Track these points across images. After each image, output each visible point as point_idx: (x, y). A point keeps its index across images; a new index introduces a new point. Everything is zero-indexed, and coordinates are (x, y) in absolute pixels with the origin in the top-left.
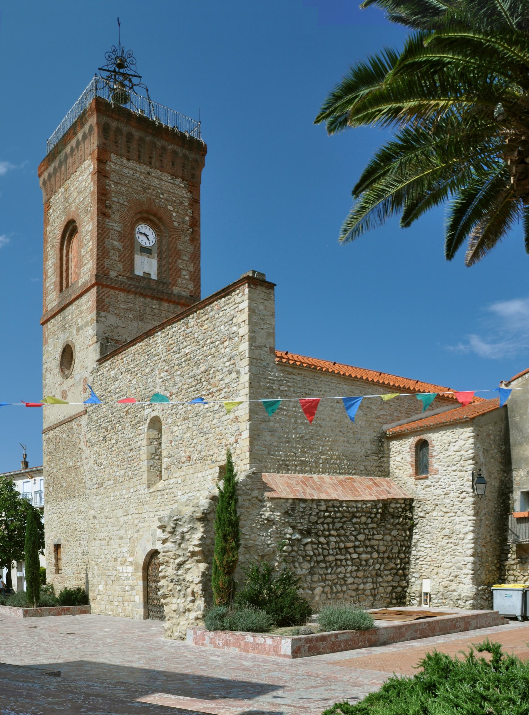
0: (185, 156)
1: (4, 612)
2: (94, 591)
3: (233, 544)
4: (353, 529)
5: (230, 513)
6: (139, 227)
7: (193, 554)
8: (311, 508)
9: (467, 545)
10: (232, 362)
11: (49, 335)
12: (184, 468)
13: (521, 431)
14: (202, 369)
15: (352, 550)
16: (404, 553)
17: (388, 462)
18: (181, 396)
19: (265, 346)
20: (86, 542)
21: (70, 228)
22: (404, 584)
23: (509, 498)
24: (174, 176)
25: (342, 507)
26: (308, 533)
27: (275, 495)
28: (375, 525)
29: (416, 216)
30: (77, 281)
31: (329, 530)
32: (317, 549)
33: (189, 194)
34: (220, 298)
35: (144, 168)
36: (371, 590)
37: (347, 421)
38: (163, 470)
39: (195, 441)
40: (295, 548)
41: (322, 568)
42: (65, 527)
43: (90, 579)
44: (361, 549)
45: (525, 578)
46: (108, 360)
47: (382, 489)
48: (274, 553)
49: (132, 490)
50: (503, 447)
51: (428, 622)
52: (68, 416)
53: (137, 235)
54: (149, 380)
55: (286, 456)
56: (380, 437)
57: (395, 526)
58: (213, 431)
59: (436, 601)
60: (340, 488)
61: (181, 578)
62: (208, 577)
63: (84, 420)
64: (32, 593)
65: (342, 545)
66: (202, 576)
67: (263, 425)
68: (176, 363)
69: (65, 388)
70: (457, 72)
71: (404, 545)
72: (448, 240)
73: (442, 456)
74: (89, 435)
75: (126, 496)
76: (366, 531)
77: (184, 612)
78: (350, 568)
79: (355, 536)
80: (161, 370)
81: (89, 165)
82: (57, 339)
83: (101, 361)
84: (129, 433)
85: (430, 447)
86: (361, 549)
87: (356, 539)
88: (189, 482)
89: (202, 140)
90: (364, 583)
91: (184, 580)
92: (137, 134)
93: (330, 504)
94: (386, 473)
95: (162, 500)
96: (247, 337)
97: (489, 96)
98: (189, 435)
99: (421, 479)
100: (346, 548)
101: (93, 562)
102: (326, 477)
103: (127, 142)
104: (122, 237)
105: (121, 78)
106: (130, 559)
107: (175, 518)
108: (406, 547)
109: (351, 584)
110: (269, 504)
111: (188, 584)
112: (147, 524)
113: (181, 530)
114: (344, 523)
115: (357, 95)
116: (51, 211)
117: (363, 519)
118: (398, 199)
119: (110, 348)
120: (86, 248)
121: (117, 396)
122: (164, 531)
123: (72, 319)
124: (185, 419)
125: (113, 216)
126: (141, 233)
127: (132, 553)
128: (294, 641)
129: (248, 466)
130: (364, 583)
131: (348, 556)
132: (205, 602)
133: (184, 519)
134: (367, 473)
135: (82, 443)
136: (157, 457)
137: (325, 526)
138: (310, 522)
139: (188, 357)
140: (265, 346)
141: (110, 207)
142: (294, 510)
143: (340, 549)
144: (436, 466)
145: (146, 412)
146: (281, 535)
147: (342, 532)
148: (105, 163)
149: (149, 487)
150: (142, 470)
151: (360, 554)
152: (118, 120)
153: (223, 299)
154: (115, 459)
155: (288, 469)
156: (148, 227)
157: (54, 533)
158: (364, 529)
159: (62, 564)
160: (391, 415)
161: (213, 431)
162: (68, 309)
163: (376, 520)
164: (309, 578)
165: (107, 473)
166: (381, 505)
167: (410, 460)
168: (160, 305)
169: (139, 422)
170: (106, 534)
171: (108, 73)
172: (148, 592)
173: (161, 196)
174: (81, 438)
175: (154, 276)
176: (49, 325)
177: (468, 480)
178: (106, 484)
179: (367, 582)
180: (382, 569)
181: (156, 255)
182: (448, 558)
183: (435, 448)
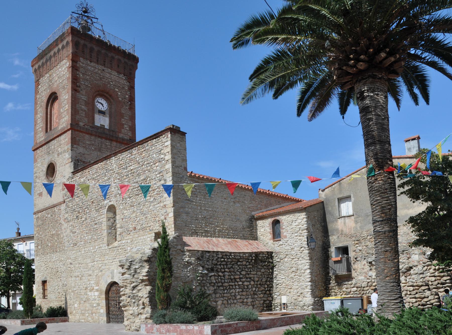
0: (125, 62)
1: (6, 323)
2: (71, 308)
3: (169, 274)
5: (166, 257)
6: (98, 99)
7: (143, 281)
8: (213, 256)
9: (307, 275)
10: (161, 174)
11: (38, 157)
12: (132, 234)
13: (333, 215)
14: (142, 178)
15: (238, 280)
16: (269, 282)
17: (256, 232)
18: (128, 193)
19: (181, 166)
20: (65, 279)
21: (53, 97)
22: (271, 299)
23: (328, 251)
24: (119, 73)
25: (231, 256)
26: (212, 270)
27: (191, 249)
29: (281, 94)
30: (58, 127)
31: (224, 269)
32: (218, 279)
34: (153, 139)
35: (101, 67)
36: (251, 302)
37: (231, 209)
38: (117, 236)
39: (138, 219)
40: (205, 278)
41: (221, 290)
42: (50, 270)
43: (68, 301)
44: (244, 280)
45: (341, 293)
46: (79, 172)
48: (192, 281)
49: (97, 247)
50: (323, 224)
51: (289, 317)
52: (52, 204)
53: (96, 104)
55: (196, 227)
57: (263, 266)
58: (150, 213)
59: (290, 307)
60: (229, 246)
61: (135, 295)
62: (152, 294)
63: (63, 207)
64: (28, 310)
65: (232, 277)
66: (149, 294)
67: (182, 210)
70: (306, 24)
71: (269, 277)
72: (298, 107)
73: (288, 228)
74: (66, 215)
75: (93, 251)
76: (246, 270)
77: (138, 315)
78: (238, 290)
79: (240, 272)
80: (115, 178)
81: (66, 63)
83: (74, 173)
84: (94, 214)
85: (281, 224)
86: (244, 280)
88: (135, 242)
89: (135, 54)
90: (247, 299)
91: (137, 296)
92: (96, 48)
93: (224, 254)
94: (255, 238)
95: (118, 252)
96: (170, 161)
97: (323, 38)
98: (134, 215)
99: (276, 241)
100: (235, 279)
101: (70, 291)
102: (220, 239)
103: (90, 52)
104: (87, 104)
105: (86, 18)
107: (130, 260)
108: (270, 279)
109: (239, 299)
110: (187, 254)
111: (140, 298)
112: (108, 267)
113: (134, 267)
114: (233, 264)
115: (254, 30)
116: (40, 86)
117: (244, 263)
118: (272, 84)
119: (80, 165)
120: (64, 108)
122: (123, 268)
123: (54, 148)
124: (131, 206)
125: (81, 92)
126: (99, 102)
127: (97, 284)
128: (212, 327)
129: (173, 233)
130: (247, 299)
131: (236, 283)
132: (151, 308)
133: (136, 261)
134: (244, 238)
135: (62, 220)
136: (113, 228)
137: (222, 266)
138: (213, 264)
139: (133, 171)
140: (181, 166)
141: (80, 87)
143: (231, 279)
144: (285, 234)
146: (195, 271)
147: (232, 270)
148: (76, 62)
149: (108, 245)
150: (104, 235)
151: (243, 282)
152: (85, 40)
153: (155, 140)
154: (85, 229)
155: (198, 235)
156: (103, 100)
157: (42, 274)
158: (245, 268)
159: (47, 293)
160: (256, 207)
161: (150, 213)
162: (51, 142)
164: (214, 296)
165: (79, 237)
166: (254, 255)
167: (269, 231)
168: (111, 143)
170: (79, 273)
171: (78, 15)
172: (109, 307)
173: (111, 83)
175: (107, 127)
176: (38, 151)
177: (304, 241)
178: (79, 244)
179: (248, 298)
181: (108, 115)
182: (296, 283)
183: (284, 224)
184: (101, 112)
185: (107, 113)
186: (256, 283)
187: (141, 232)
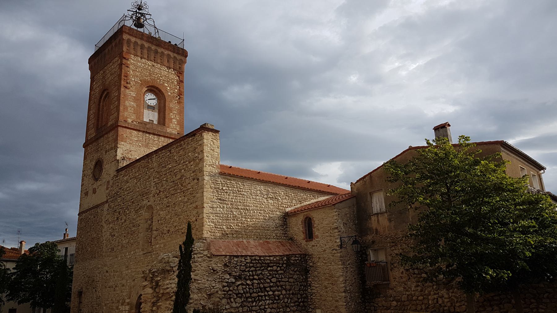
14: (178, 177)
24: (169, 68)
28: (282, 272)
35: (149, 63)
39: (172, 220)
40: (231, 288)
41: (249, 302)
54: (147, 183)
63: (106, 206)
65: (262, 286)
69: (95, 186)
75: (128, 257)
76: (277, 276)
87: (271, 281)
92: (146, 45)
100: (265, 288)
106: (127, 301)
117: (275, 268)
123: (103, 145)
131: (266, 293)
143: (260, 288)
144: (317, 233)
145: (144, 202)
151: (274, 291)
163: (283, 268)
185: (157, 107)
186: (288, 292)
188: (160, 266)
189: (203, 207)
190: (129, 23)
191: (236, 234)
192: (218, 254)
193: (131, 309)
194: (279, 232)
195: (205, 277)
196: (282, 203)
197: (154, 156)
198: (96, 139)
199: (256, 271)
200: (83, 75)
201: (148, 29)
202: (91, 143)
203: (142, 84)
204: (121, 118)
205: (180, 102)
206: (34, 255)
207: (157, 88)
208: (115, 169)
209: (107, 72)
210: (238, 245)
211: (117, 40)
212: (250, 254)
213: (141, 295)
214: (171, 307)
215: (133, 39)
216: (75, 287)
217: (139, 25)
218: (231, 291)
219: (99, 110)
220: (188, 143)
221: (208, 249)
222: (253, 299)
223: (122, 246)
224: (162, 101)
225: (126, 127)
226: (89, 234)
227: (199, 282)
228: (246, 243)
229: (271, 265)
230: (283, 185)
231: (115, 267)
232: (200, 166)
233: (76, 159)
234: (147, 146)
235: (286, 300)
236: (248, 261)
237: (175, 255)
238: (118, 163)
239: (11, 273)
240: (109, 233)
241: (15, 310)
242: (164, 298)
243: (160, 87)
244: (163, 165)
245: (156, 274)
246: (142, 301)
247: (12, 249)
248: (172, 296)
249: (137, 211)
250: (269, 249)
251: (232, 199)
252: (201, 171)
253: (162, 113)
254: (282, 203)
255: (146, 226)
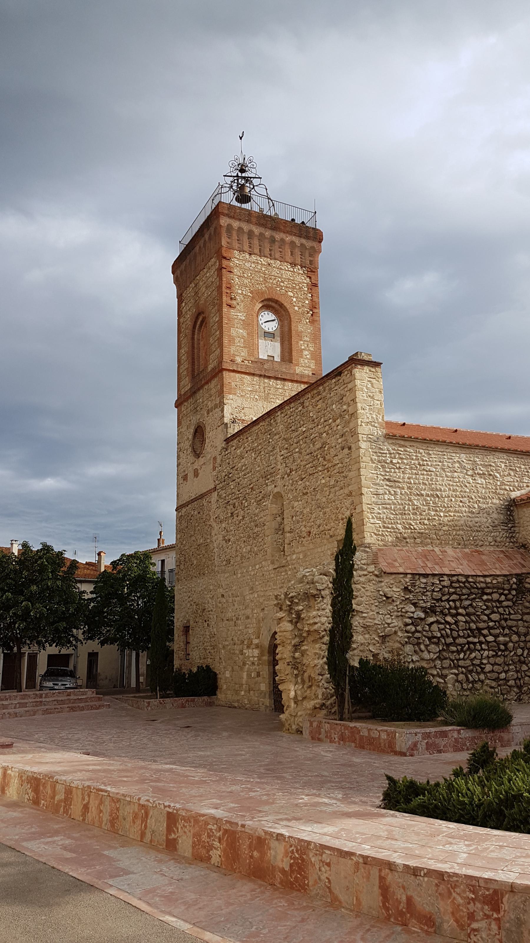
4: (485, 607)
6: (262, 314)
15: (485, 632)
24: (293, 264)
26: (432, 611)
28: (510, 603)
31: (456, 608)
33: (308, 279)
35: (263, 261)
36: (515, 680)
40: (419, 628)
41: (453, 652)
44: (498, 631)
47: (515, 561)
54: (271, 458)
56: (508, 505)
68: (295, 441)
75: (252, 573)
76: (501, 610)
81: (215, 262)
82: (190, 421)
86: (498, 631)
87: (489, 619)
90: (506, 672)
92: (257, 230)
100: (479, 629)
106: (256, 641)
109: (489, 672)
117: (495, 596)
121: (243, 473)
123: (203, 402)
131: (482, 639)
135: (212, 520)
142: (415, 586)
143: (470, 629)
145: (269, 488)
154: (242, 535)
169: (263, 498)
171: (231, 179)
174: (211, 515)
179: (509, 670)
180: (525, 655)
181: (279, 339)
184: (268, 335)
185: (278, 334)
187: (318, 540)
188: (301, 588)
189: (362, 494)
190: (229, 198)
191: (422, 537)
192: (392, 570)
193: (262, 654)
194: (501, 534)
195: (374, 608)
196: (502, 484)
197: (279, 413)
198: (193, 392)
199: (461, 600)
200: (164, 293)
201: (254, 206)
202: (186, 400)
203: (253, 298)
204: (226, 358)
205: (314, 320)
206: (119, 572)
207: (276, 302)
208: (223, 438)
209: (201, 283)
210: (425, 556)
211: (212, 229)
212: (448, 572)
213: (275, 633)
214: (322, 653)
215: (236, 224)
216: (179, 619)
217: (244, 198)
218: (419, 632)
219: (193, 347)
220: (330, 389)
221: (375, 562)
222: (459, 647)
223: (242, 557)
224: (286, 323)
225: (234, 371)
226: (193, 538)
227: (364, 615)
228: (438, 553)
229: (488, 591)
230: (503, 450)
231: (234, 588)
232: (352, 425)
233: (165, 425)
234: (266, 398)
235: (519, 652)
236: (445, 583)
237: (323, 572)
238: (227, 428)
239: (89, 599)
240: (221, 536)
241: (98, 653)
242: (310, 639)
243: (282, 300)
244: (293, 428)
245: (296, 601)
246: (277, 642)
247: (87, 563)
248: (323, 636)
249: (259, 503)
250: (483, 563)
251: (409, 478)
252: (354, 433)
253: (286, 342)
254: (502, 484)
255: (274, 525)
